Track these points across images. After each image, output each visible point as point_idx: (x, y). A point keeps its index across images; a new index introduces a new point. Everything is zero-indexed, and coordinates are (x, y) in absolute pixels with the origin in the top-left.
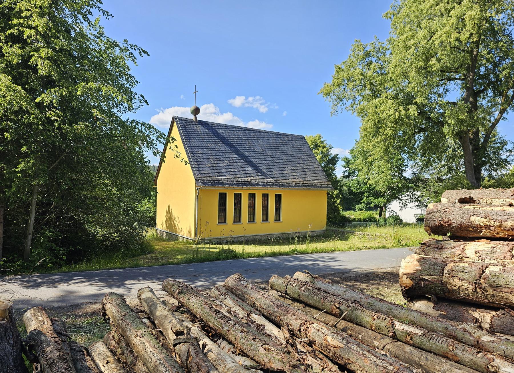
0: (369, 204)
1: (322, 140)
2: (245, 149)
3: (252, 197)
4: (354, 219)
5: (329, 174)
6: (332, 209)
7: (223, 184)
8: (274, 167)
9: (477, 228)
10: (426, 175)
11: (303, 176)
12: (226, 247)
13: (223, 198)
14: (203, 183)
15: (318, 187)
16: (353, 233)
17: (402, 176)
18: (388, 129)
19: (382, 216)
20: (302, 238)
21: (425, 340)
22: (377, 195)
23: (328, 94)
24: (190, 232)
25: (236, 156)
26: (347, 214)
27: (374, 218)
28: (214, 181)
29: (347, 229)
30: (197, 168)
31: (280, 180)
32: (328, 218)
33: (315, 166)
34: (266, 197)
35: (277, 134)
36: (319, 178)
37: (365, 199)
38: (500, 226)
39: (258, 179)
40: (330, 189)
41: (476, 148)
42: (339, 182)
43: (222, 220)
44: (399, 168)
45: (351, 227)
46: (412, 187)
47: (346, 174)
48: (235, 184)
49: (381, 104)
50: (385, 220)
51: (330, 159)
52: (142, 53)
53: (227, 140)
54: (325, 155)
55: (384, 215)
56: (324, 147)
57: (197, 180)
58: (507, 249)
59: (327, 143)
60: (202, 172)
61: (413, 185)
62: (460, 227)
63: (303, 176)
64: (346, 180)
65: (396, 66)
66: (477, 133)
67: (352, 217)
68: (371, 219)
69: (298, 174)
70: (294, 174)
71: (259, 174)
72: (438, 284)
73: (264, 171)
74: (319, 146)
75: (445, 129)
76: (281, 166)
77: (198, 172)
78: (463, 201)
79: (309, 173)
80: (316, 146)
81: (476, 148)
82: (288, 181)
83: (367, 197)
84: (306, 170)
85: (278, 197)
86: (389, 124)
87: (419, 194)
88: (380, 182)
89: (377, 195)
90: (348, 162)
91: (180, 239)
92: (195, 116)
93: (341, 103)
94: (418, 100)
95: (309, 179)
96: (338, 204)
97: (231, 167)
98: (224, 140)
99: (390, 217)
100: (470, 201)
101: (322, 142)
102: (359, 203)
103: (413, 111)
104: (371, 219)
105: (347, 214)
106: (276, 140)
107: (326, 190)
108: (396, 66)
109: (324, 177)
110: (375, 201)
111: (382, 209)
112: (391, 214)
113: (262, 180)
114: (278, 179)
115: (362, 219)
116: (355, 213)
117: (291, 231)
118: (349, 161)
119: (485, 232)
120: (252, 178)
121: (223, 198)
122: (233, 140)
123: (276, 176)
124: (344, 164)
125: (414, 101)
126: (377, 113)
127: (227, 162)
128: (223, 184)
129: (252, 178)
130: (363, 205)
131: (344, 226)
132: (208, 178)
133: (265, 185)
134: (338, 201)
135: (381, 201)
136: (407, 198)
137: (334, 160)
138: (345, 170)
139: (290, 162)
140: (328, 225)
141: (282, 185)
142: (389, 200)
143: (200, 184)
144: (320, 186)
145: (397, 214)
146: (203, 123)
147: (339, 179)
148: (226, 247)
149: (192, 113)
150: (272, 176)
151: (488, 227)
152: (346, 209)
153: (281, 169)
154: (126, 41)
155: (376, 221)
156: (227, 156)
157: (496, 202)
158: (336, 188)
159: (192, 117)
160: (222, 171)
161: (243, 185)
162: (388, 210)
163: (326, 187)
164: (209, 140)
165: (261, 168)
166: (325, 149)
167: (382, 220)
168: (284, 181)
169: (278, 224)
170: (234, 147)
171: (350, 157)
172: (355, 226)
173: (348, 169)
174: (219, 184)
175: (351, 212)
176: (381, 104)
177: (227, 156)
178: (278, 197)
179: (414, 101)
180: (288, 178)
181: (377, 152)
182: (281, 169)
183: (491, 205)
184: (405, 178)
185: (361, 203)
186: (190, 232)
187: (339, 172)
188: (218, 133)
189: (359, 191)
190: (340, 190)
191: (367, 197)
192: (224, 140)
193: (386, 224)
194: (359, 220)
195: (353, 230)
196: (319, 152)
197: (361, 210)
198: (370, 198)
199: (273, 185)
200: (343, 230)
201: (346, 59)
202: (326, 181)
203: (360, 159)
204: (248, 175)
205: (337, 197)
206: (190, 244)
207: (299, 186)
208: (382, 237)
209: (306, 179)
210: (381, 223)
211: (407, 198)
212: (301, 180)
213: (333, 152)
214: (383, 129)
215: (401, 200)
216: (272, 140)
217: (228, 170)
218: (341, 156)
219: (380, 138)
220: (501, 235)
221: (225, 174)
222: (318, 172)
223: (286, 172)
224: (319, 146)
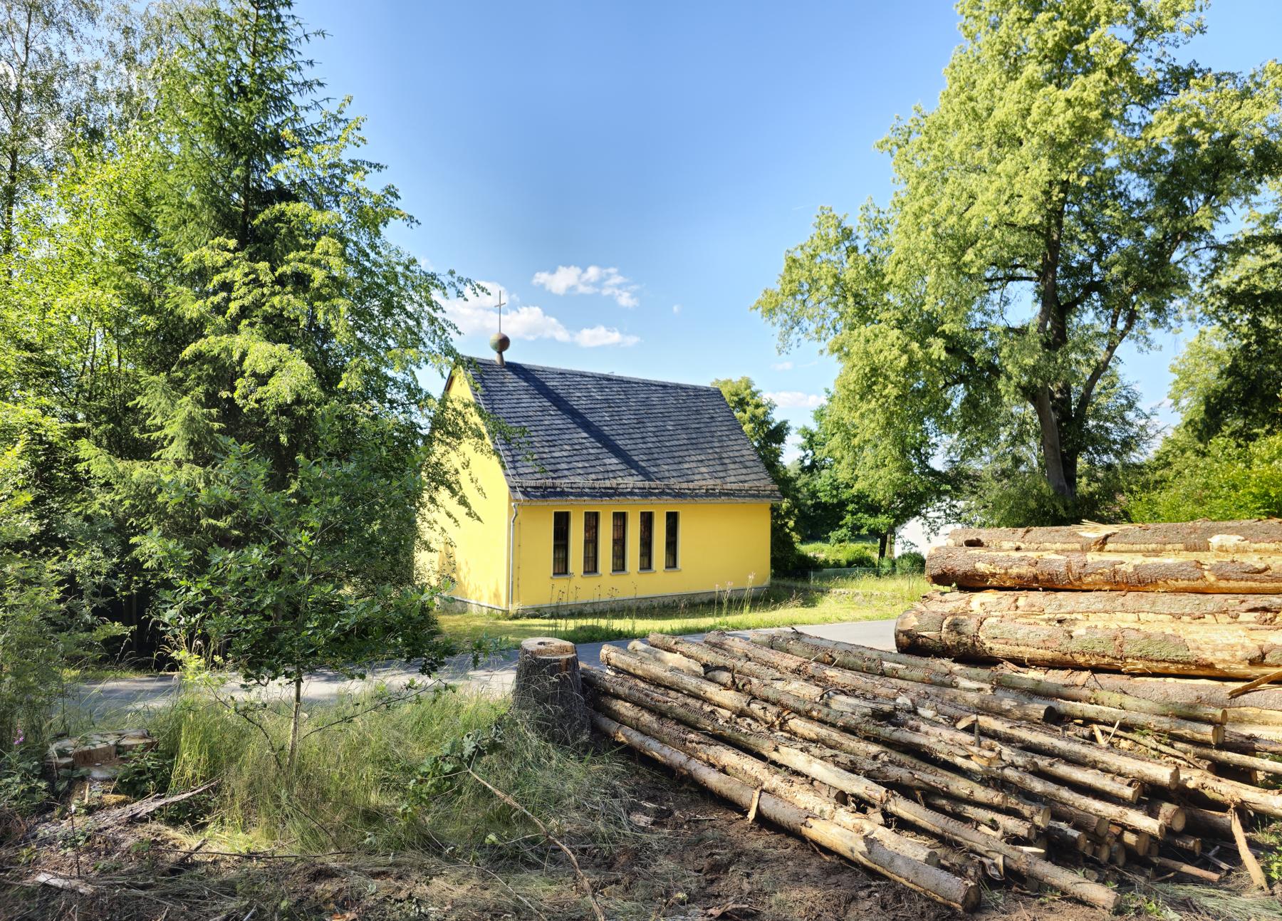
0: (856, 528)
1: (753, 389)
2: (601, 418)
3: (620, 519)
4: (826, 562)
5: (771, 463)
6: (780, 542)
7: (563, 494)
8: (661, 456)
9: (984, 577)
10: (975, 465)
11: (721, 474)
12: (590, 622)
13: (562, 523)
14: (525, 493)
15: (753, 496)
16: (824, 592)
17: (928, 467)
18: (890, 386)
19: (887, 553)
20: (736, 603)
21: (907, 672)
22: (874, 510)
23: (771, 312)
24: (496, 596)
25: (585, 435)
26: (812, 550)
27: (868, 560)
28: (546, 488)
29: (814, 583)
30: (511, 464)
31: (676, 484)
32: (774, 562)
33: (745, 452)
34: (647, 519)
35: (664, 386)
36: (753, 477)
37: (848, 518)
38: (1006, 574)
39: (631, 481)
40: (775, 501)
41: (1065, 416)
42: (792, 480)
43: (561, 567)
44: (920, 450)
45: (822, 579)
46: (946, 492)
47: (807, 462)
48: (587, 495)
49: (876, 336)
50: (894, 564)
51: (771, 431)
52: (478, 291)
53: (566, 402)
54: (761, 423)
55: (891, 552)
56: (757, 406)
57: (513, 488)
58: (1012, 599)
59: (765, 397)
60: (521, 471)
61: (949, 487)
62: (965, 575)
63: (721, 474)
64: (805, 478)
65: (899, 262)
66: (1066, 389)
67: (822, 556)
68: (861, 563)
69: (711, 469)
70: (704, 470)
71: (633, 471)
72: (937, 639)
73: (643, 464)
74: (748, 404)
75: (1001, 384)
76: (676, 454)
77: (514, 472)
78: (971, 544)
79: (732, 466)
80: (742, 403)
81: (1065, 416)
82: (691, 485)
83: (853, 514)
84: (727, 461)
85: (672, 519)
86: (892, 376)
87: (961, 504)
88: (879, 486)
89: (874, 510)
90: (811, 441)
91: (474, 610)
92: (500, 353)
93: (797, 329)
94: (947, 328)
95: (733, 479)
96: (792, 530)
97: (577, 458)
98: (560, 403)
99: (904, 556)
100: (975, 543)
101: (754, 395)
102: (836, 526)
103: (937, 348)
104: (861, 563)
105: (812, 550)
106: (662, 399)
107: (767, 504)
108: (899, 262)
109: (763, 475)
110: (869, 521)
111: (883, 538)
112: (906, 551)
113: (640, 484)
114: (672, 481)
115: (844, 562)
116: (826, 547)
117: (717, 588)
118: (812, 436)
119: (991, 581)
120: (620, 480)
121: (562, 523)
122: (579, 401)
123: (667, 474)
124: (802, 441)
125: (940, 329)
126: (867, 353)
127: (568, 447)
128: (563, 494)
129: (620, 480)
130: (844, 530)
131: (805, 577)
132: (533, 483)
133: (646, 494)
134: (791, 524)
135: (882, 521)
136: (937, 514)
137: (778, 434)
138: (803, 454)
139: (694, 444)
140: (774, 576)
141: (679, 495)
142: (902, 517)
143: (519, 496)
144: (757, 495)
145: (917, 550)
146: (515, 368)
147: (791, 474)
148: (590, 622)
149: (495, 347)
150: (659, 476)
151: (994, 575)
152: (807, 539)
153: (676, 460)
154: (452, 273)
155: (873, 565)
156: (567, 436)
157: (1006, 545)
158: (785, 495)
159: (493, 356)
160: (559, 466)
161: (603, 495)
162: (898, 541)
163: (768, 496)
164: (531, 404)
165: (636, 458)
166: (760, 411)
167: (886, 563)
168: (684, 485)
169: (672, 575)
170: (581, 416)
171: (814, 427)
172: (828, 578)
173: (810, 452)
174: (556, 494)
175: (819, 545)
176: (876, 336)
177: (567, 436)
178: (672, 519)
179: (940, 329)
180: (692, 477)
181: (870, 427)
182: (676, 460)
183: (1000, 549)
184: (934, 473)
185: (841, 527)
186: (496, 596)
187: (791, 455)
188: (546, 388)
189: (835, 501)
190: (795, 499)
191: (853, 514)
192: (560, 403)
193: (894, 571)
194: (837, 564)
195: (826, 584)
196: (747, 416)
197: (841, 541)
198: (860, 515)
199: (663, 493)
200: (805, 585)
201: (805, 240)
202: (767, 484)
203: (838, 438)
204: (611, 475)
205: (789, 513)
206: (498, 618)
207: (713, 495)
208: (885, 599)
209: (728, 479)
210: (885, 570)
211: (937, 514)
212: (718, 481)
213: (777, 417)
214: (880, 387)
215: (925, 518)
216: (655, 398)
217: (571, 466)
218: (795, 423)
219: (873, 403)
220: (1008, 584)
221: (566, 473)
222: (751, 464)
223: (686, 466)
224: (748, 404)
